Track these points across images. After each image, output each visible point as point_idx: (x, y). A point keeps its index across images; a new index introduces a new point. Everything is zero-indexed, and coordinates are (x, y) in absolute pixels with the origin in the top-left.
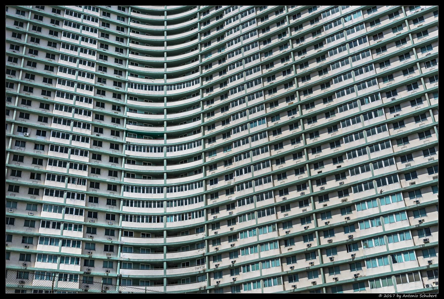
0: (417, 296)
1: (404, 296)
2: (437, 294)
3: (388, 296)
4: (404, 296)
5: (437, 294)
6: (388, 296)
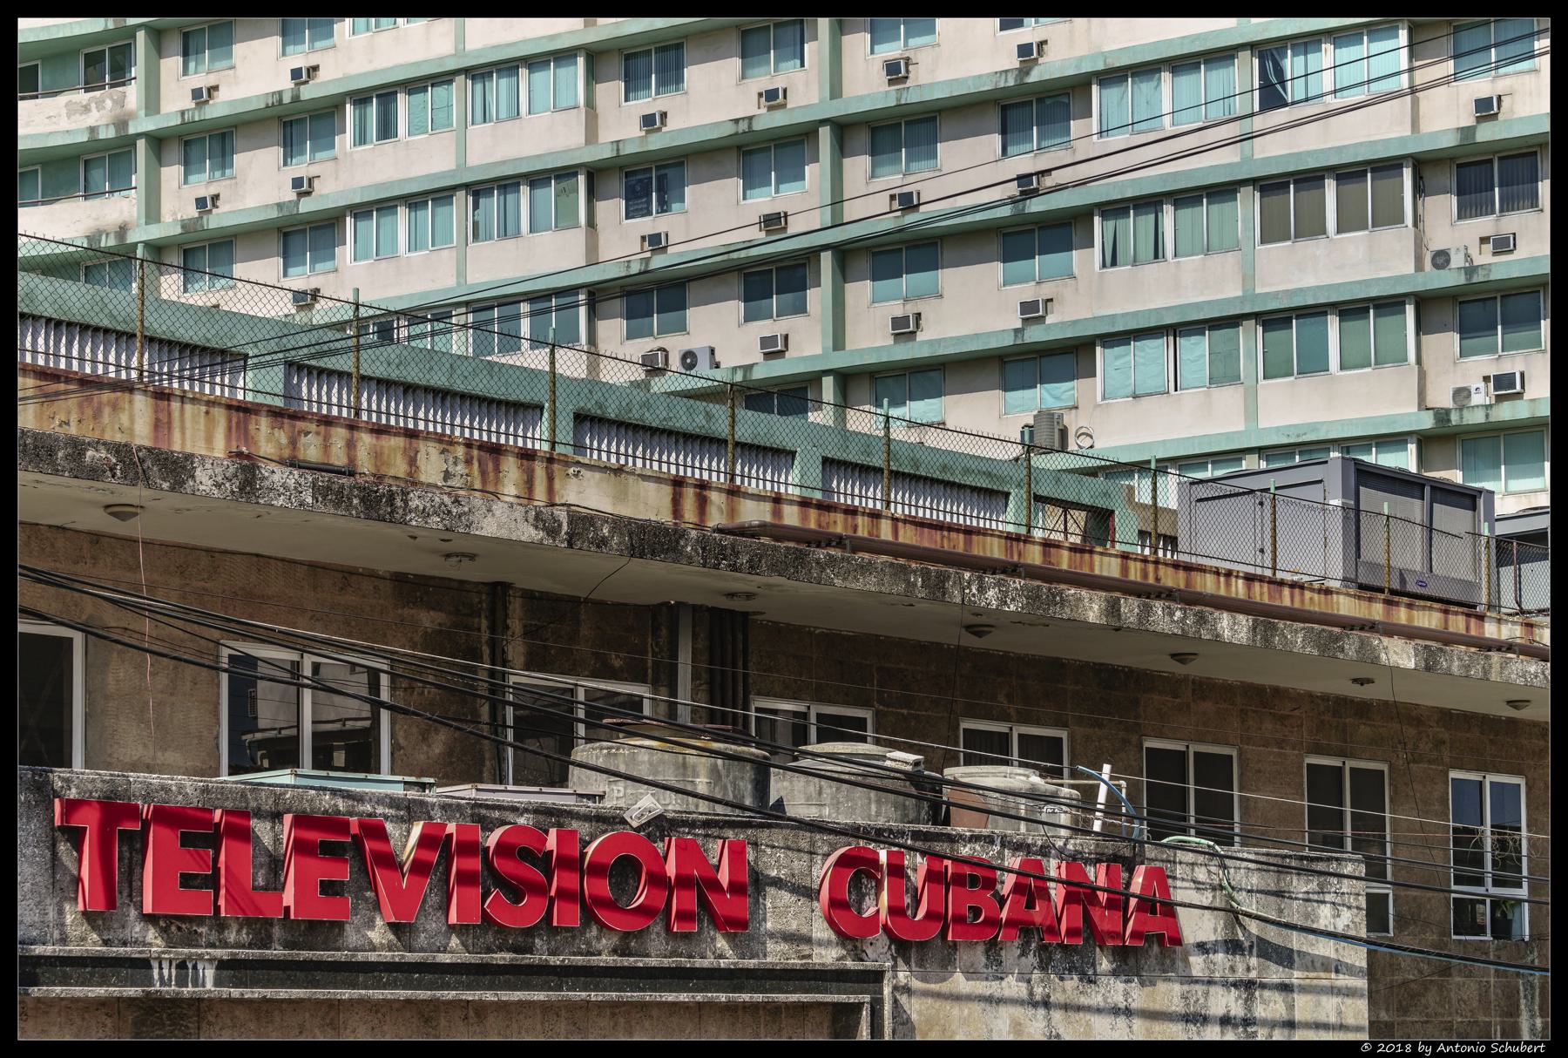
0: (1482, 1049)
1: (1441, 1048)
2: (1545, 1043)
3: (1391, 1048)
4: (1441, 1048)
5: (1545, 1043)
6: (1391, 1048)
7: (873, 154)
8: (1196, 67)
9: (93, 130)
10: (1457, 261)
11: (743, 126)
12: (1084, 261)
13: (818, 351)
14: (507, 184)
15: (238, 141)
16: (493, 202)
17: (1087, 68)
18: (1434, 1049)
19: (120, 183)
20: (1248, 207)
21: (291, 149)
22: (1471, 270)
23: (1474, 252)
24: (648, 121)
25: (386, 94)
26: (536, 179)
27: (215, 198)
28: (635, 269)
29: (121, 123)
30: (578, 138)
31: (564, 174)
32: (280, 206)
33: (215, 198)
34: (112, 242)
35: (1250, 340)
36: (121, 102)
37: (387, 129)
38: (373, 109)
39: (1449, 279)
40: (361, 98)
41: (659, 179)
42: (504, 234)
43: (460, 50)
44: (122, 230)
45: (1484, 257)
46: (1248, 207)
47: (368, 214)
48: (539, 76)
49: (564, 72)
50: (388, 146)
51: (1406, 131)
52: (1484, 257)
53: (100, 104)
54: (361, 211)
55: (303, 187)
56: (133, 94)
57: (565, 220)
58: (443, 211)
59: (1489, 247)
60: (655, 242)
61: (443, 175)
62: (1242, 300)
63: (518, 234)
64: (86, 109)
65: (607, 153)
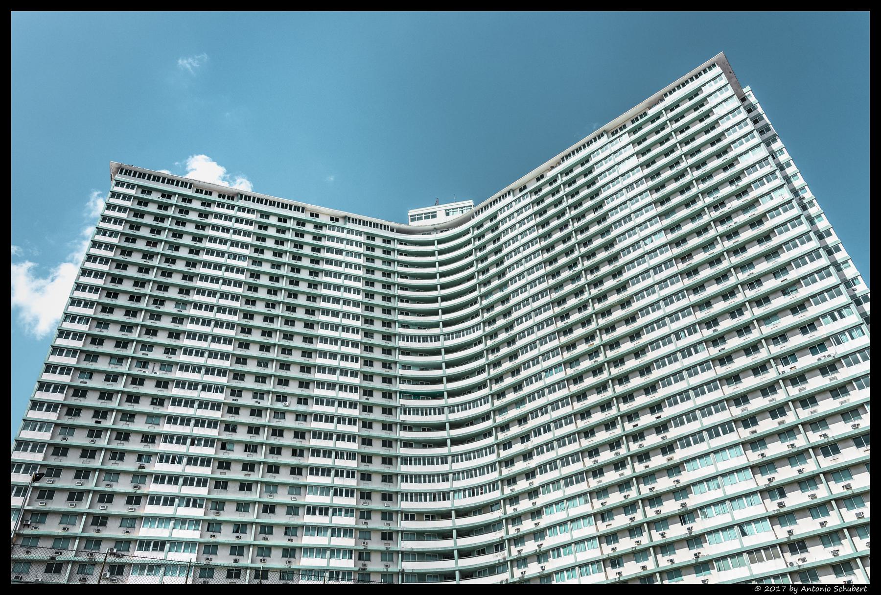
7: (662, 554)
8: (718, 504)
9: (499, 560)
10: (795, 565)
11: (634, 549)
12: (714, 572)
13: (654, 568)
14: (586, 565)
15: (528, 560)
16: (584, 569)
17: (703, 531)
18: (799, 590)
19: (504, 571)
20: (624, 190)
21: (539, 562)
22: (799, 566)
23: (798, 562)
24: (613, 549)
25: (558, 548)
26: (592, 563)
27: (525, 572)
28: (617, 580)
29: (504, 558)
30: (600, 554)
31: (598, 561)
32: (539, 573)
33: (525, 572)
34: (503, 561)
35: (656, 287)
36: (504, 554)
37: (559, 556)
38: (556, 552)
39: (795, 568)
40: (553, 550)
41: (618, 561)
42: (587, 575)
43: (540, 352)
44: (507, 580)
45: (800, 563)
46: (624, 190)
47: (547, 507)
48: (585, 520)
49: (594, 542)
50: (560, 558)
51: (689, 302)
52: (800, 563)
53: (500, 555)
54: (550, 528)
55: (543, 568)
56: (506, 552)
57: (599, 570)
58: (574, 572)
59: (801, 561)
60: (595, 462)
61: (573, 564)
62: (750, 576)
63: (590, 574)
64: (497, 556)
65: (607, 557)
